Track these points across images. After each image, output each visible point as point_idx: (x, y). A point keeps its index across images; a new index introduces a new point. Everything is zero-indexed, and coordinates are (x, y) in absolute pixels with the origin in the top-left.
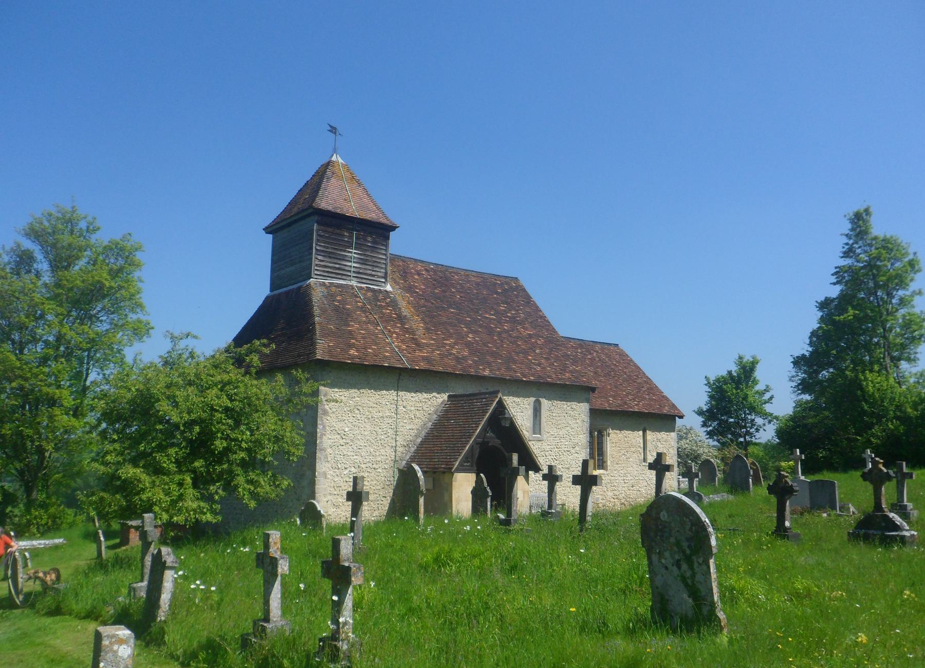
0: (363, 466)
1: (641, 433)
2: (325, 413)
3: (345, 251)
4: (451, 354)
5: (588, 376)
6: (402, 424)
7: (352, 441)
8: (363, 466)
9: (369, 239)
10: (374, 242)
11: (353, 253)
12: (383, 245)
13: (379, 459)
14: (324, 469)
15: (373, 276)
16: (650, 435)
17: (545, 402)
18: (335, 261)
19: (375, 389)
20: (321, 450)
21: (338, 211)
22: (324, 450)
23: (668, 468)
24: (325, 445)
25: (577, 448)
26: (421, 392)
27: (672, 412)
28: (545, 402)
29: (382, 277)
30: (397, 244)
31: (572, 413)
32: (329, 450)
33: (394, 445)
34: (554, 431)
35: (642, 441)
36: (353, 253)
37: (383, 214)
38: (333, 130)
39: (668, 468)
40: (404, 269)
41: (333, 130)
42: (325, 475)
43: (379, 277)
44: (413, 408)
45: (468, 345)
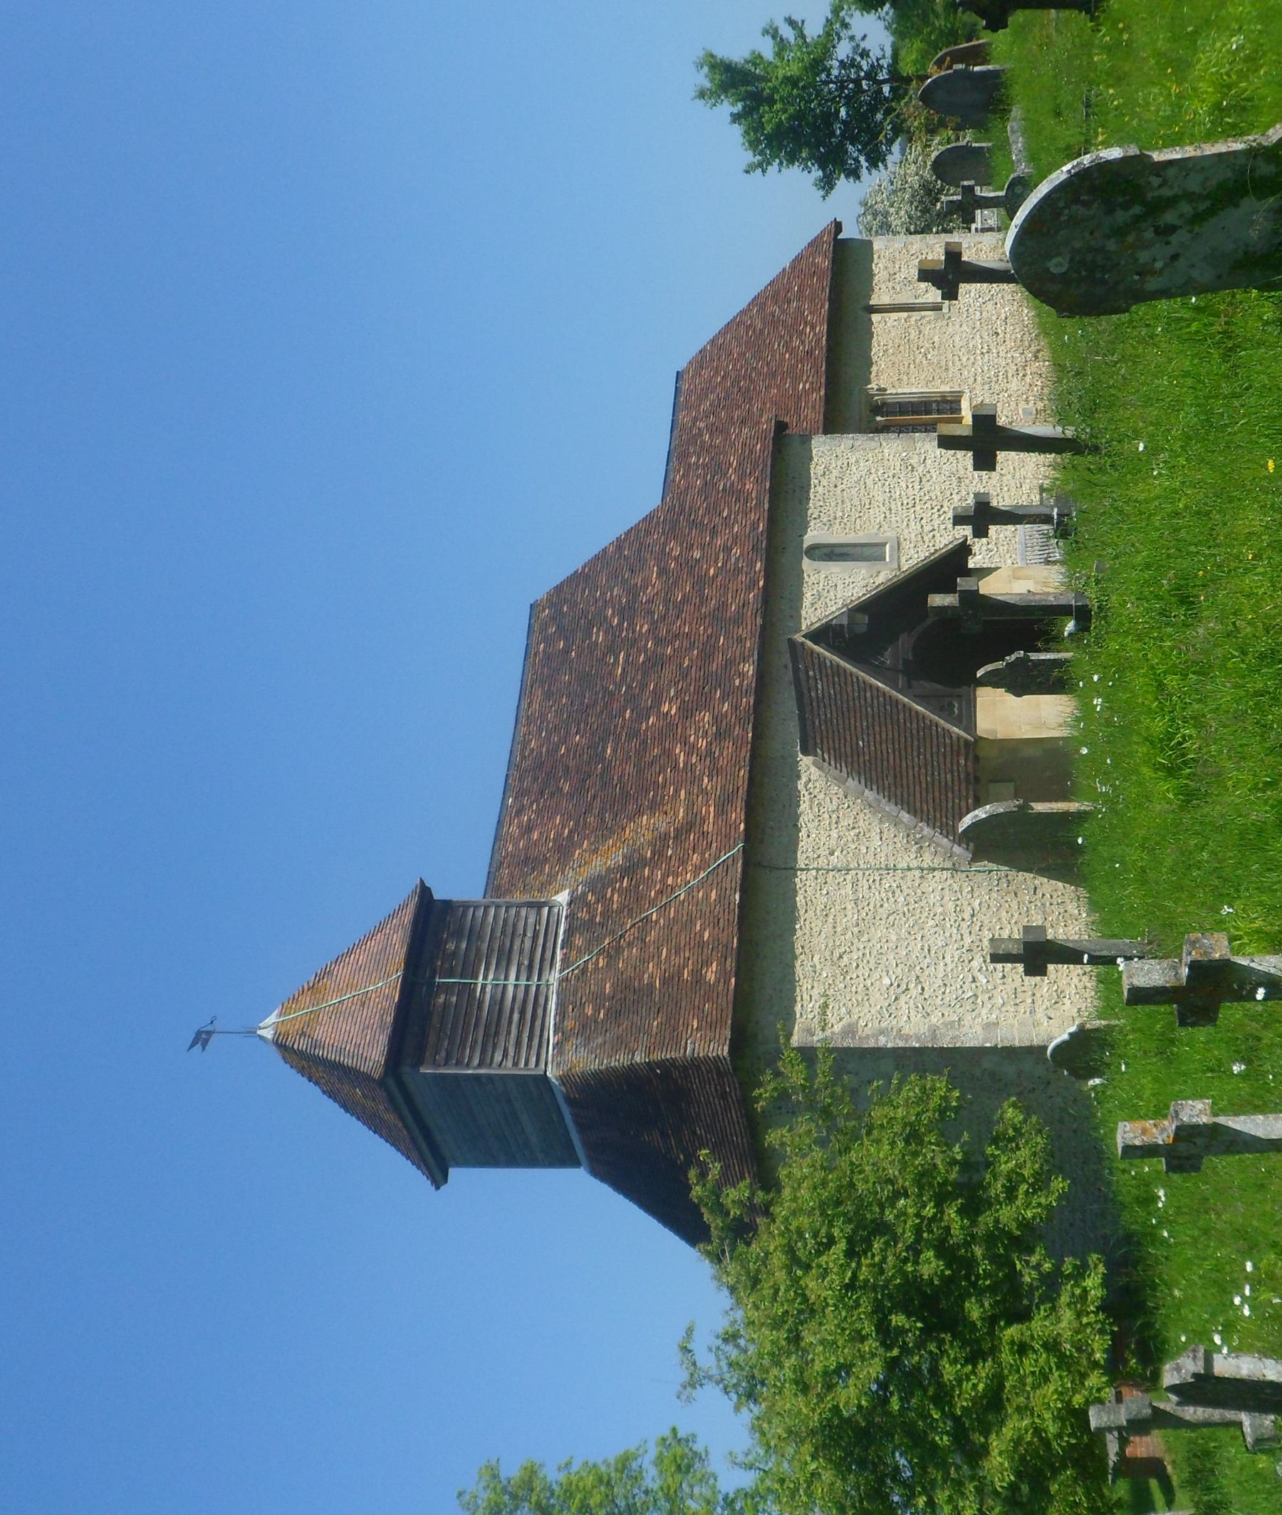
0: (968, 940)
1: (875, 318)
2: (850, 1030)
3: (481, 1002)
4: (710, 753)
5: (752, 438)
6: (870, 858)
7: (911, 968)
8: (968, 940)
9: (451, 946)
10: (458, 934)
11: (485, 981)
12: (464, 915)
13: (951, 906)
14: (979, 1029)
15: (529, 1047)
16: (881, 296)
17: (813, 535)
18: (504, 1022)
19: (795, 920)
20: (934, 1037)
21: (389, 1019)
22: (934, 1031)
23: (953, 255)
24: (924, 1029)
25: (914, 461)
26: (797, 817)
27: (827, 247)
28: (813, 535)
29: (539, 914)
30: (461, 882)
31: (835, 473)
32: (935, 1019)
33: (917, 873)
34: (877, 514)
35: (894, 316)
36: (485, 981)
37: (392, 916)
38: (202, 1038)
39: (953, 255)
40: (516, 865)
41: (202, 1038)
42: (990, 1026)
43: (538, 922)
44: (834, 834)
45: (687, 712)
